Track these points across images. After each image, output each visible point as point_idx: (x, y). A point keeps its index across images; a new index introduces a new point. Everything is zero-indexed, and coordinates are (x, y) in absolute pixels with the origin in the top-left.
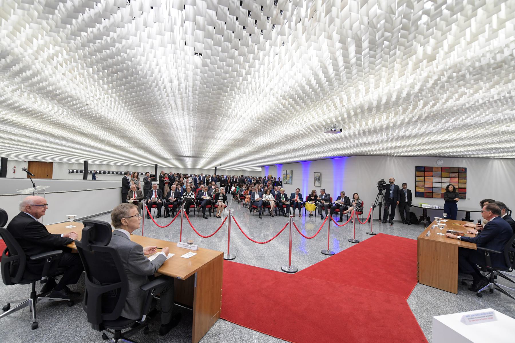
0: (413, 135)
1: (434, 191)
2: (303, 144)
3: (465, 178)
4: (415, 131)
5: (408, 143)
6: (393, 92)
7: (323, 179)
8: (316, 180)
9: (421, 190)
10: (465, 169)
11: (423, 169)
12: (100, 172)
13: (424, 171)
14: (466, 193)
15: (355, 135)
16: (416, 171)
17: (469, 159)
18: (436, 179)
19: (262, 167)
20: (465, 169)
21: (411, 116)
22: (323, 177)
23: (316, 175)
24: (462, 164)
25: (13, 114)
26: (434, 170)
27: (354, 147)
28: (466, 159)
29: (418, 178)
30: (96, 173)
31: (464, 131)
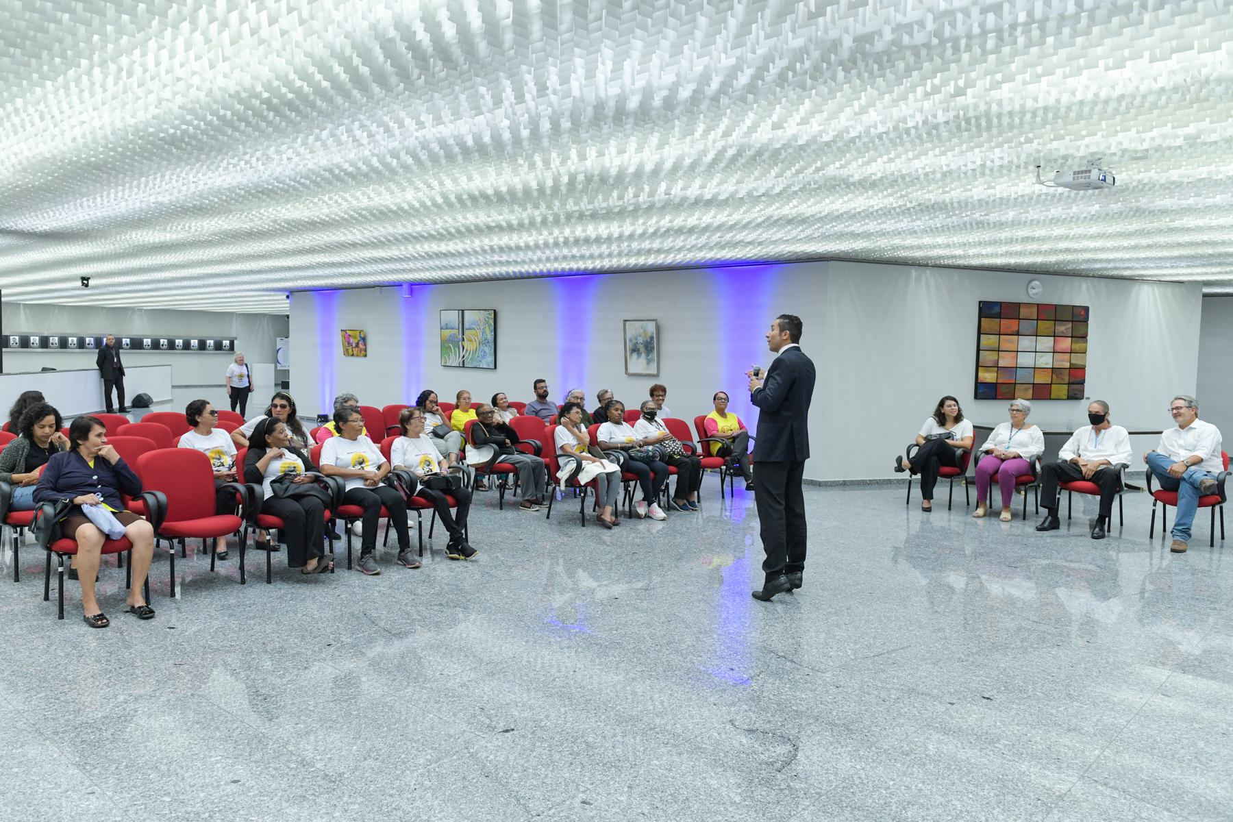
0: (722, 197)
1: (1021, 377)
2: (365, 202)
3: (1084, 337)
4: (728, 188)
5: (722, 217)
6: (660, 89)
7: (669, 346)
8: (635, 350)
9: (988, 377)
10: (1087, 309)
11: (997, 309)
12: (137, 344)
13: (999, 316)
14: (1082, 382)
15: (556, 188)
16: (981, 315)
17: (1096, 281)
18: (1025, 342)
19: (291, 293)
20: (1087, 309)
21: (720, 145)
22: (665, 336)
23: (634, 330)
24: (1075, 294)
25: (737, 176)
26: (1024, 312)
27: (557, 221)
28: (1089, 281)
29: (987, 340)
30: (118, 344)
31: (842, 196)
